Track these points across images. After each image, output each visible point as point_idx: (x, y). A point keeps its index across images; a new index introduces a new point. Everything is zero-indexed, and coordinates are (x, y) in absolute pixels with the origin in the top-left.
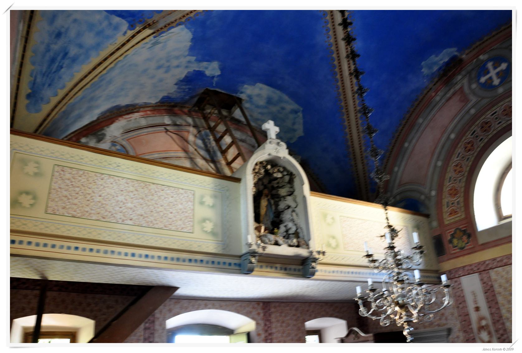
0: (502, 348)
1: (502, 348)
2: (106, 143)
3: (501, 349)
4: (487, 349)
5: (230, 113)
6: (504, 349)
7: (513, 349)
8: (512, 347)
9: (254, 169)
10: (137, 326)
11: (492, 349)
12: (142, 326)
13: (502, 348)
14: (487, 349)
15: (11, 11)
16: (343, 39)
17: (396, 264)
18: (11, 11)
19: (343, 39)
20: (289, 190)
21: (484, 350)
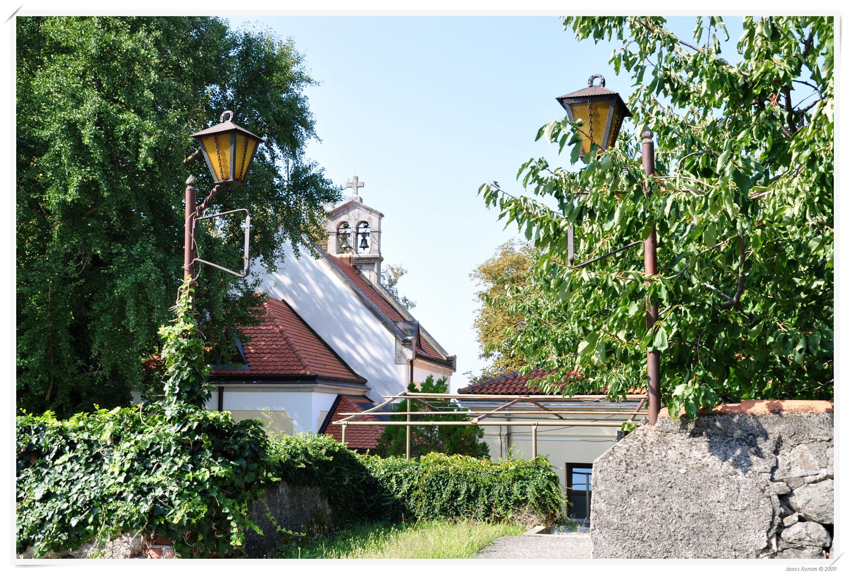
0: (818, 567)
1: (818, 567)
2: (833, 123)
3: (815, 568)
4: (793, 569)
5: (797, 270)
6: (821, 569)
7: (835, 569)
8: (833, 566)
9: (832, 126)
10: (72, 415)
11: (800, 569)
12: (77, 415)
13: (818, 567)
14: (793, 569)
15: (18, 18)
16: (484, 271)
17: (244, 531)
18: (18, 18)
19: (484, 271)
20: (755, 21)
21: (789, 569)
